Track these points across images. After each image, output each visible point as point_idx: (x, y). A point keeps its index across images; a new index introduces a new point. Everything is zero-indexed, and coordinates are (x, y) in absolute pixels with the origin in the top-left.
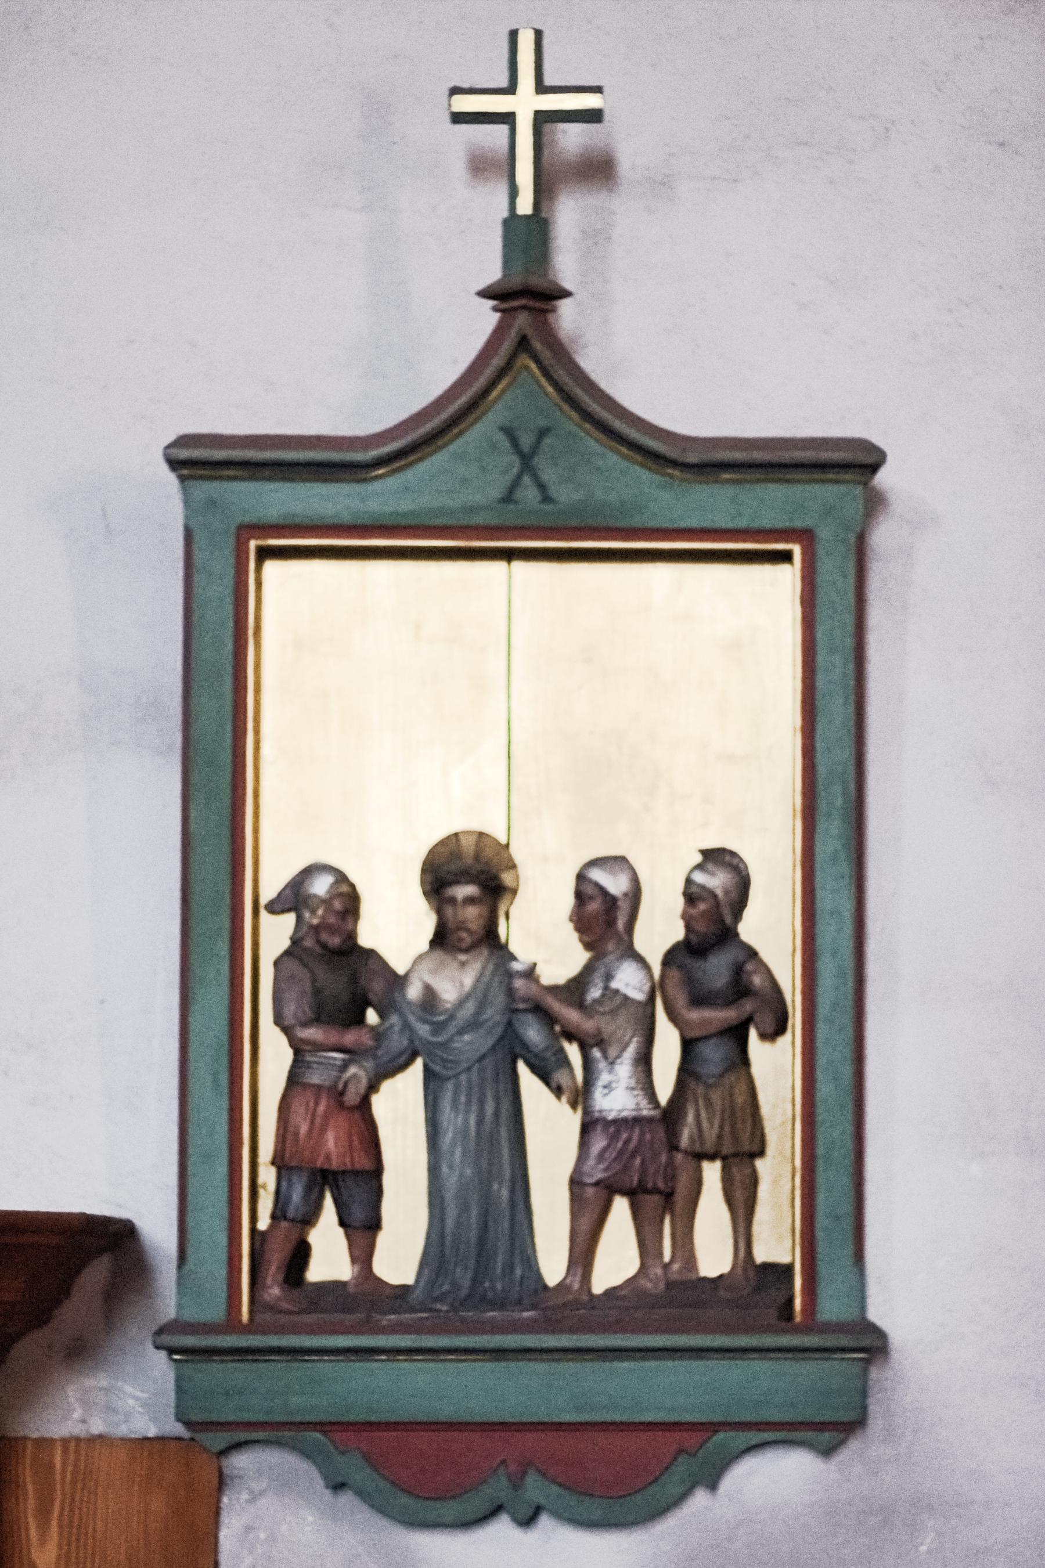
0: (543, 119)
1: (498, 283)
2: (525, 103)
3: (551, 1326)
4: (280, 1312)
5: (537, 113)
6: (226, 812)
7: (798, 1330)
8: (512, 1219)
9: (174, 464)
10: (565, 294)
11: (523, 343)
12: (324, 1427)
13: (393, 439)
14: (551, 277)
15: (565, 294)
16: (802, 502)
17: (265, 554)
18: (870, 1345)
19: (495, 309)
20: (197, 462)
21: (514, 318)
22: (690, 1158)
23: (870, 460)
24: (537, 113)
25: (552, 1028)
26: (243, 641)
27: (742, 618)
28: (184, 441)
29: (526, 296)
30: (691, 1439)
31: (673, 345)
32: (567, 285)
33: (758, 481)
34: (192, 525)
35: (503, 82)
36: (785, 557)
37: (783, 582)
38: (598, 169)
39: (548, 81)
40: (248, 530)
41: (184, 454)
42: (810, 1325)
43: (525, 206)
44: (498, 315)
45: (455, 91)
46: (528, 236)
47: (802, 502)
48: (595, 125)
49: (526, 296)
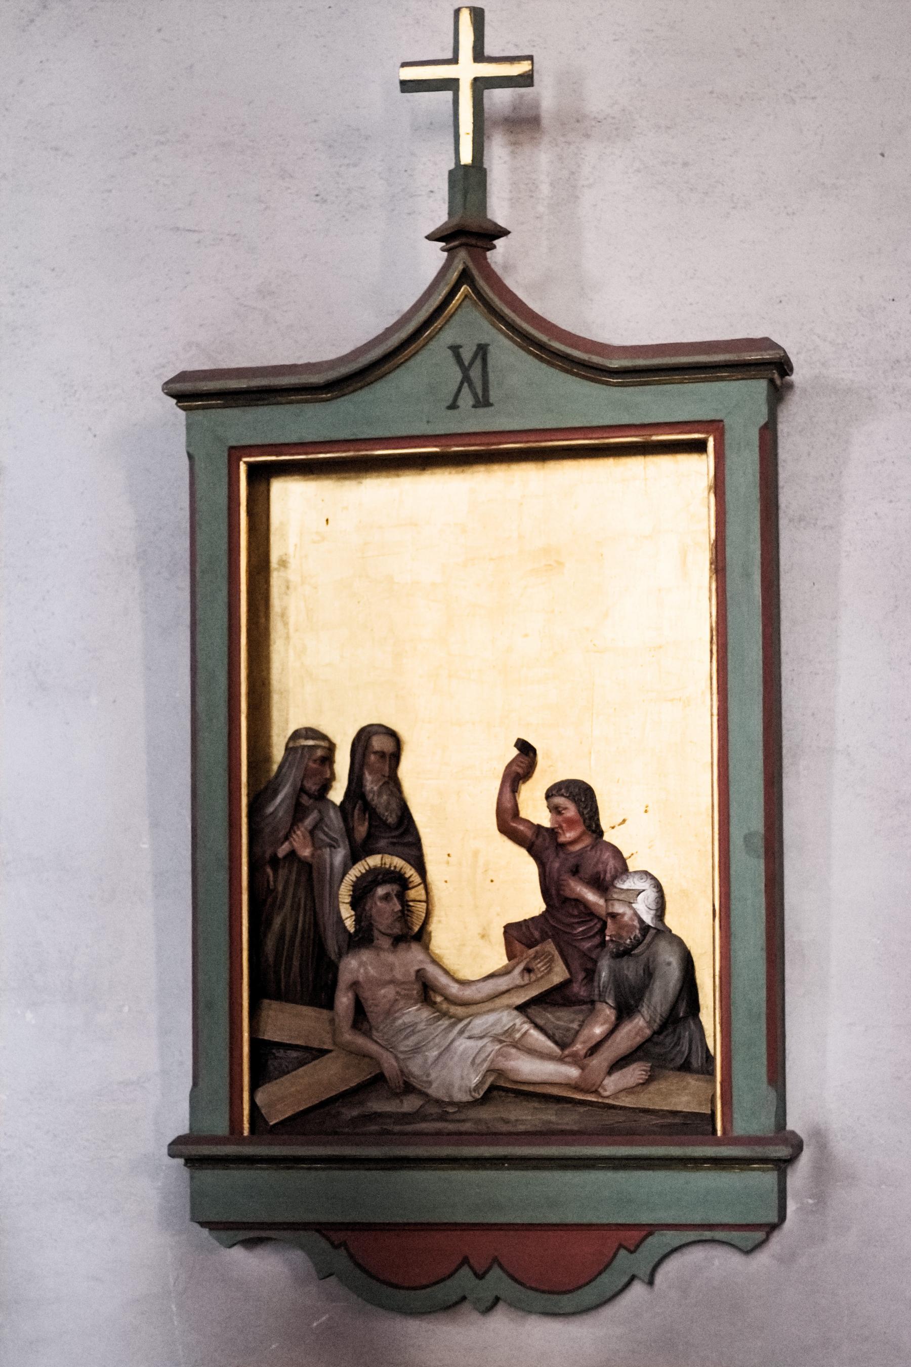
0: (480, 85)
1: (446, 223)
2: (467, 71)
3: (610, 1134)
4: (395, 1134)
5: (457, 81)
7: (719, 1143)
9: (181, 397)
10: (504, 233)
11: (465, 277)
12: (321, 1228)
13: (707, 353)
14: (489, 216)
15: (504, 233)
16: (723, 398)
18: (779, 1152)
19: (443, 250)
20: (193, 393)
22: (515, 1013)
24: (476, 80)
28: (183, 376)
29: (469, 235)
31: (614, 269)
32: (502, 222)
33: (307, 401)
34: (191, 452)
35: (449, 55)
36: (698, 447)
37: (699, 468)
38: (524, 124)
39: (489, 51)
40: (235, 453)
41: (187, 387)
42: (729, 1139)
43: (466, 157)
44: (446, 254)
46: (469, 182)
49: (469, 235)
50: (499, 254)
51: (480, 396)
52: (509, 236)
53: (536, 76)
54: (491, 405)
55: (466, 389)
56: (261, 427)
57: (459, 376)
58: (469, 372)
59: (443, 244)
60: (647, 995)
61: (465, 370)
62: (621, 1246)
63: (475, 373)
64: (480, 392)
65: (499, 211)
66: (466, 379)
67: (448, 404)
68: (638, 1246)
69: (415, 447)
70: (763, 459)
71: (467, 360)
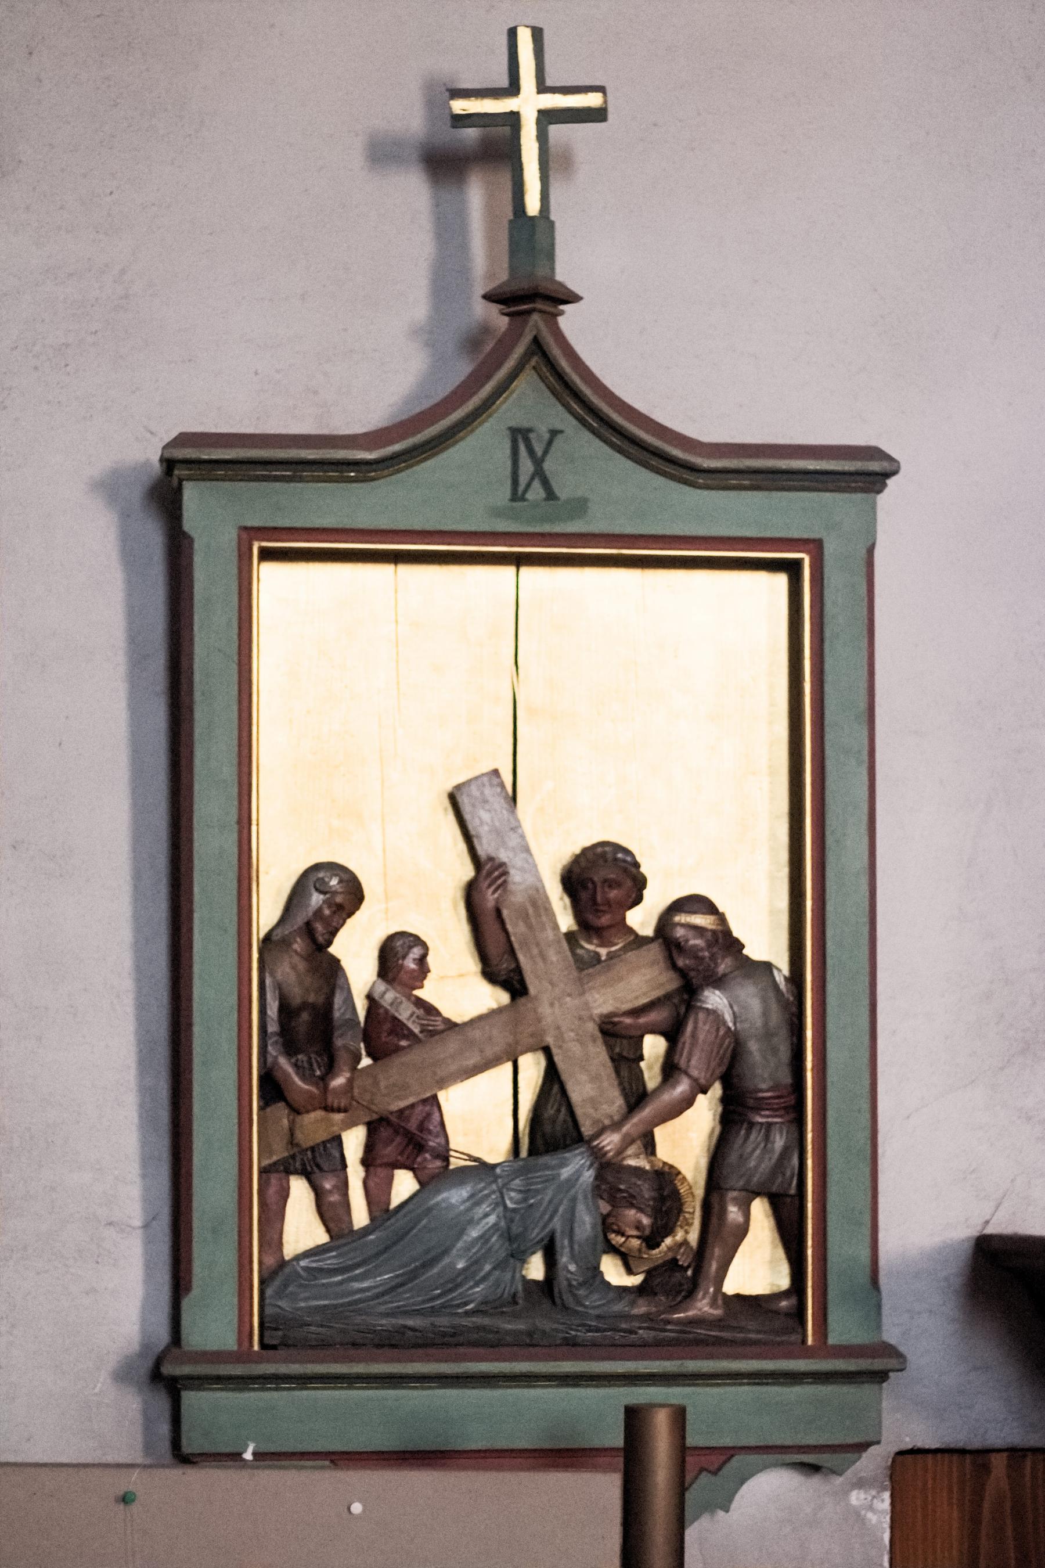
2: (528, 104)
5: (540, 112)
6: (865, 818)
7: (802, 1351)
8: (735, 1328)
10: (572, 298)
13: (582, 378)
15: (572, 298)
16: (795, 509)
17: (267, 555)
21: (526, 322)
23: (875, 466)
24: (540, 112)
25: (404, 1048)
26: (741, 547)
27: (722, 631)
28: (184, 439)
30: (716, 1459)
39: (549, 83)
42: (823, 1350)
44: (506, 319)
45: (537, 34)
47: (795, 509)
48: (603, 124)
49: (531, 297)
50: (571, 321)
51: (522, 448)
52: (582, 302)
53: (610, 109)
54: (510, 428)
55: (539, 450)
56: (213, 512)
57: (548, 466)
58: (526, 438)
59: (502, 307)
60: (788, 1381)
61: (540, 474)
62: (702, 1470)
63: (527, 467)
64: (522, 448)
65: (567, 271)
66: (538, 463)
67: (559, 436)
68: (719, 1469)
69: (487, 545)
70: (822, 574)
71: (536, 484)
